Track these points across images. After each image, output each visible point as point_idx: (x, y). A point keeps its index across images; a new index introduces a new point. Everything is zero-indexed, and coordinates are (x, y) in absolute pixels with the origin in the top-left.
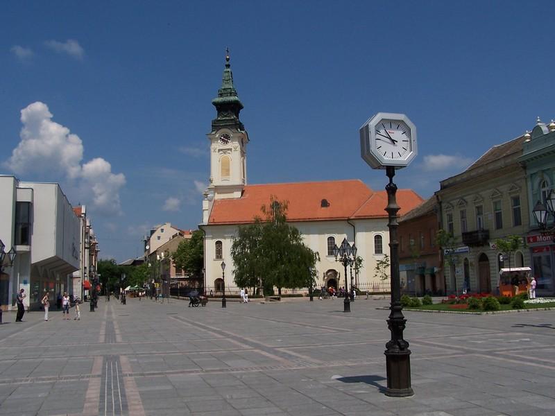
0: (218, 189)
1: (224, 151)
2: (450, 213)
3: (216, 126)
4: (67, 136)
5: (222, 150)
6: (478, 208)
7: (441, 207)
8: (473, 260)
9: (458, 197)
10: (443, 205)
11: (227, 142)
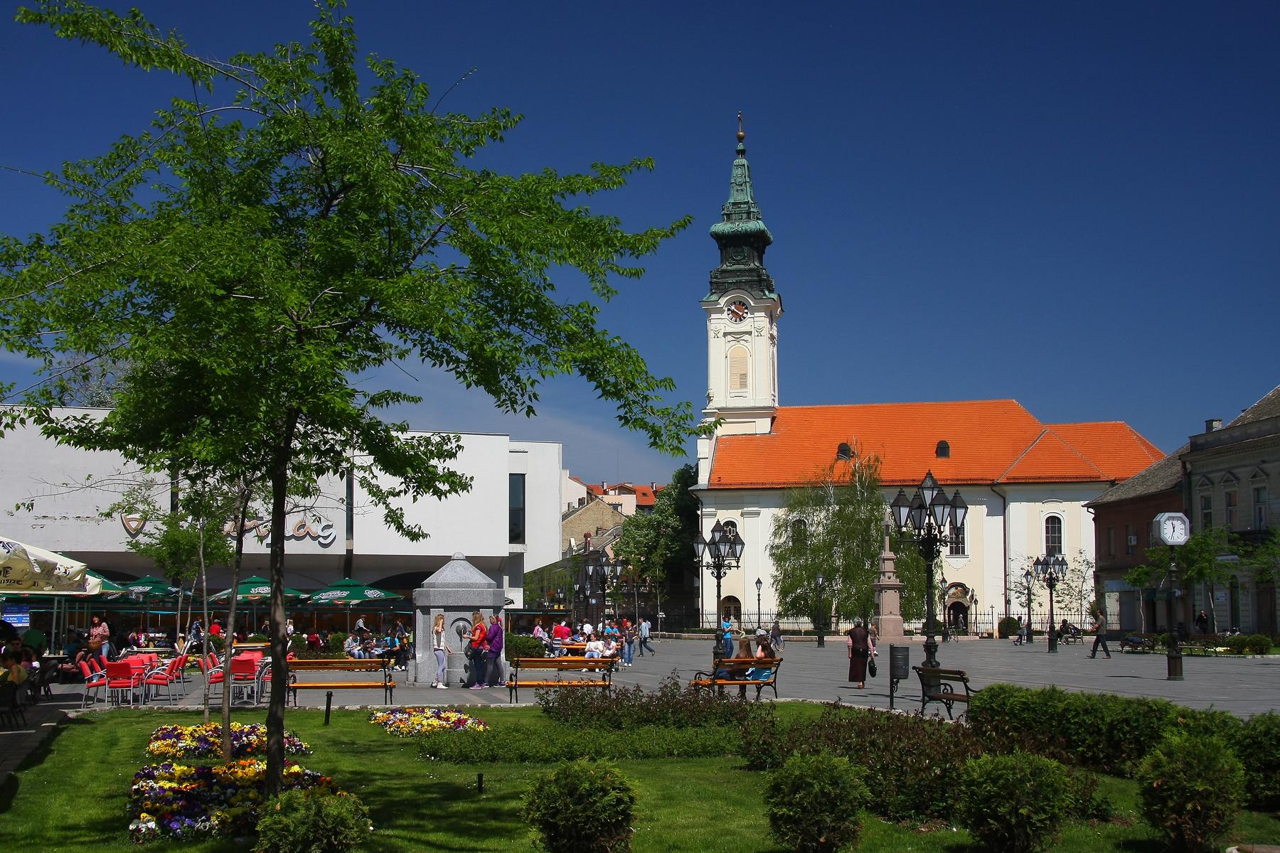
0: (724, 414)
1: (737, 336)
2: (1206, 494)
3: (719, 287)
4: (840, 699)
5: (730, 333)
6: (1257, 490)
7: (1190, 483)
8: (1246, 580)
9: (1221, 467)
10: (1195, 478)
11: (741, 318)
